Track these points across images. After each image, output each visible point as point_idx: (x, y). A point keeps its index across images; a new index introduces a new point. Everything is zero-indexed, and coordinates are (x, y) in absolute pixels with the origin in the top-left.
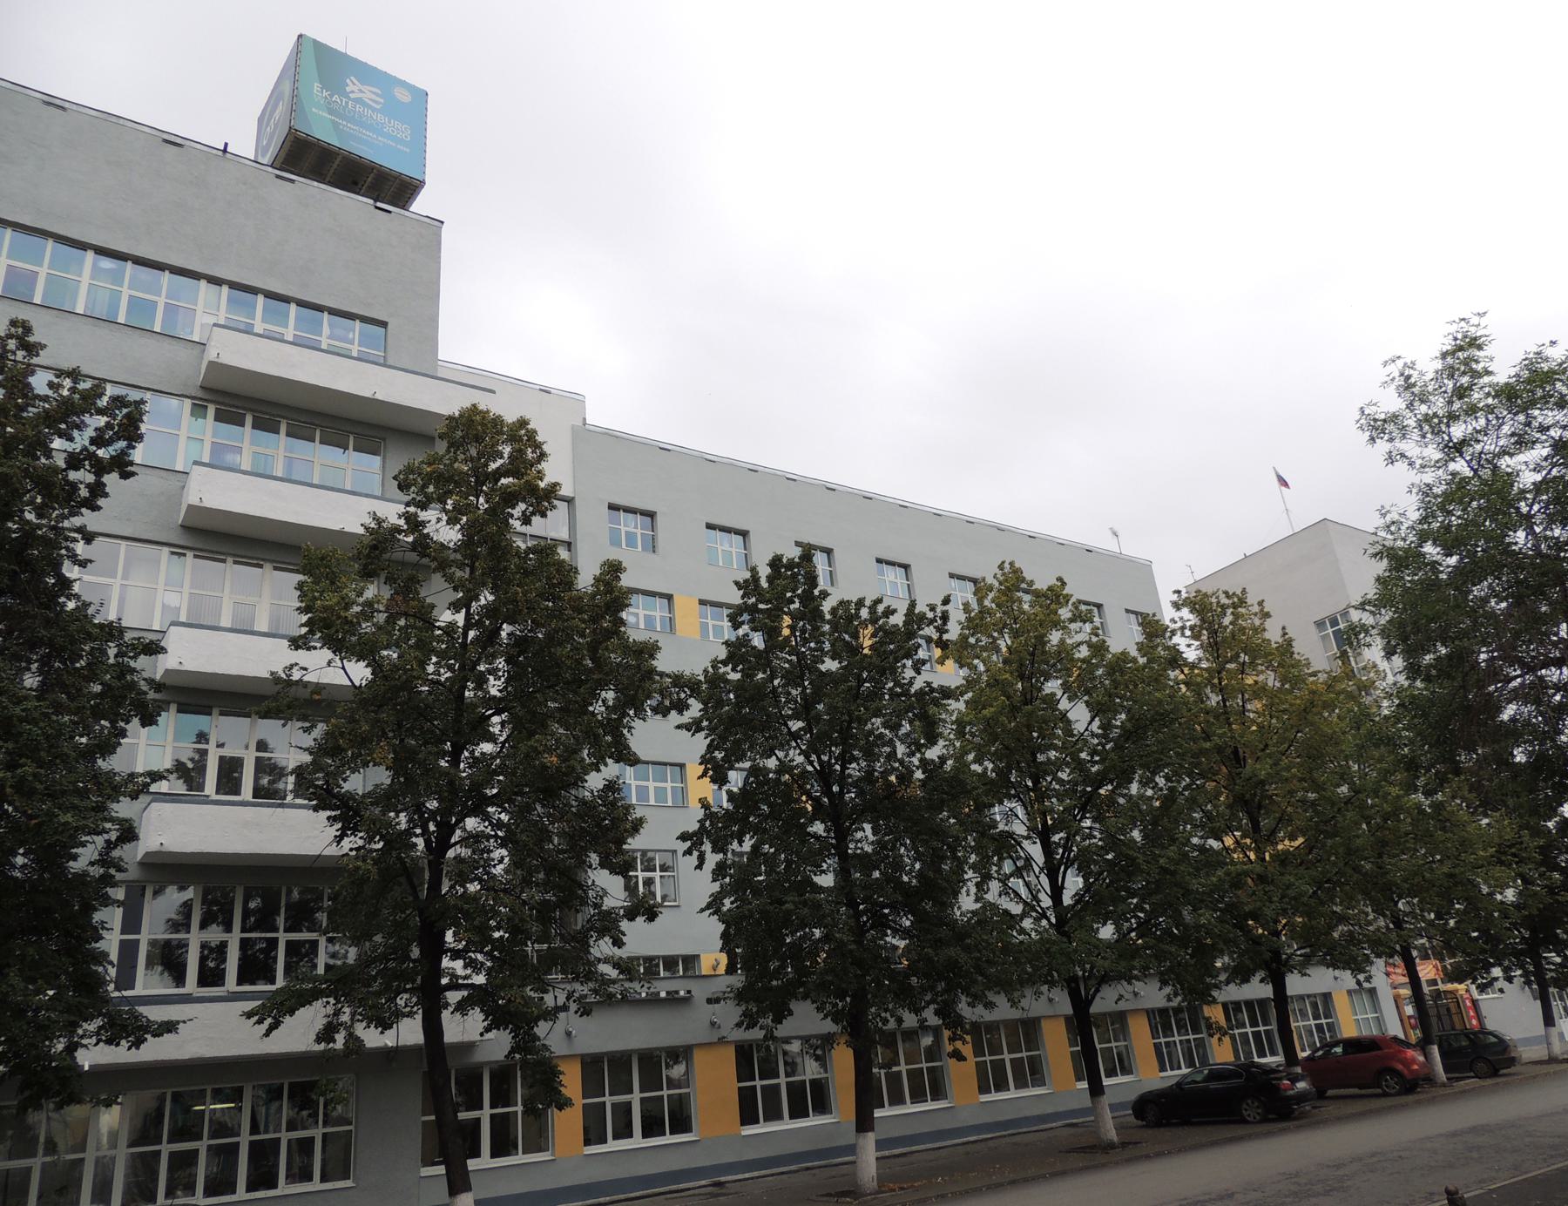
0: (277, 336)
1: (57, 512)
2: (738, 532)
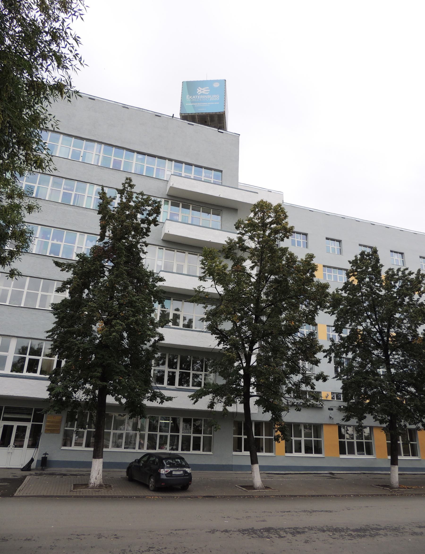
0: (189, 177)
1: (138, 237)
2: (337, 241)
